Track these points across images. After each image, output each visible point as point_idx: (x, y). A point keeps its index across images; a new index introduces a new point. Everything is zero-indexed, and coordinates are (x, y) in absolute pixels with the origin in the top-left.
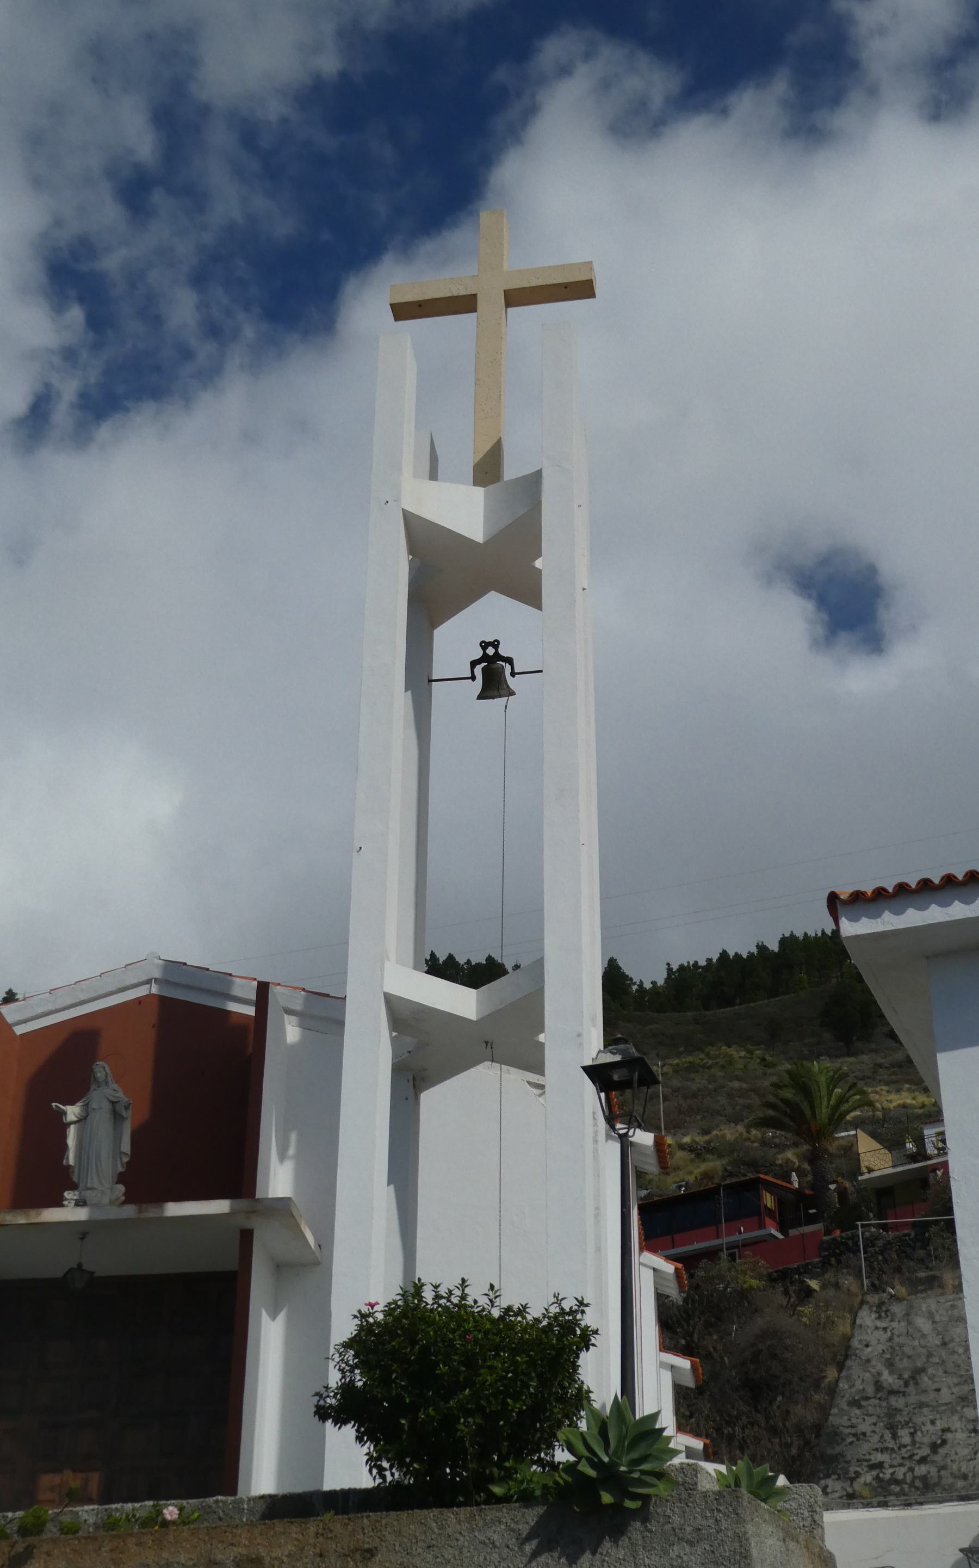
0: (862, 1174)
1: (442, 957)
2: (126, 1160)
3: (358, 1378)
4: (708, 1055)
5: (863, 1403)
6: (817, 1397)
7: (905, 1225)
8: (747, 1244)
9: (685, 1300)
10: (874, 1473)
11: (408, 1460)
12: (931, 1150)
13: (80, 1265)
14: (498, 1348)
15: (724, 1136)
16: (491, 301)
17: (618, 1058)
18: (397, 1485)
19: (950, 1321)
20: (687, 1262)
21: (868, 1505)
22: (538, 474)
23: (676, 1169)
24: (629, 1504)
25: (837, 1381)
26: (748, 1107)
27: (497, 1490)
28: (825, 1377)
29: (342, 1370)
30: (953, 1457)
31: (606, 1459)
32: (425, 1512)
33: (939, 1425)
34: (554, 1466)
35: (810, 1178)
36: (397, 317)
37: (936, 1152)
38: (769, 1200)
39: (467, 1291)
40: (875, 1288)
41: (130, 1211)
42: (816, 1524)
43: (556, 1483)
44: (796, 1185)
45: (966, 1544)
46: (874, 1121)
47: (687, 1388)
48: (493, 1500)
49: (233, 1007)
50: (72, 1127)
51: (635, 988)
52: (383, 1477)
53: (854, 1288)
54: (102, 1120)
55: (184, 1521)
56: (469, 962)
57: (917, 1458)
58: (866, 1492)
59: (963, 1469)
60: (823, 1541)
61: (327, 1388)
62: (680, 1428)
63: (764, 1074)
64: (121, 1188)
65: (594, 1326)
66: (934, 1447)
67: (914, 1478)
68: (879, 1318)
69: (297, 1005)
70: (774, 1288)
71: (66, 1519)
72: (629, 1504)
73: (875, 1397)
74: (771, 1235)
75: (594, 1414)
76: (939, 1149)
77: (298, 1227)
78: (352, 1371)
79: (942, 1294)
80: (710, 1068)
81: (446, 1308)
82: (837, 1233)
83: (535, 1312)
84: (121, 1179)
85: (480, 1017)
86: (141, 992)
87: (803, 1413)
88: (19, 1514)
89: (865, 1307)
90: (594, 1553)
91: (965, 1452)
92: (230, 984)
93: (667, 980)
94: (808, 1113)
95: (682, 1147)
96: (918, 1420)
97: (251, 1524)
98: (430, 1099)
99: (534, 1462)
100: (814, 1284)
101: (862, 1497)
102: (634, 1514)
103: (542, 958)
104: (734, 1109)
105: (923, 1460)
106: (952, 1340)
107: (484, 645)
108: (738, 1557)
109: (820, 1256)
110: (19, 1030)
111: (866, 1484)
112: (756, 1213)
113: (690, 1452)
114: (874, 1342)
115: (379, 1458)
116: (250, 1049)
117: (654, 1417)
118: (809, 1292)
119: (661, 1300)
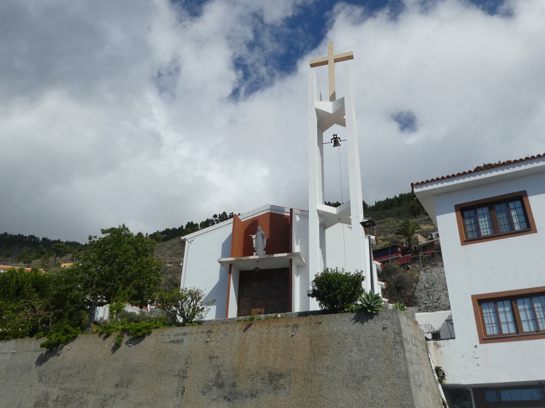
0: (419, 243)
1: (327, 202)
2: (265, 246)
3: (316, 288)
4: (385, 220)
5: (422, 291)
6: (412, 290)
7: (429, 253)
8: (395, 259)
9: (382, 271)
10: (425, 305)
11: (327, 304)
12: (434, 237)
13: (257, 267)
14: (345, 281)
15: (389, 237)
16: (331, 62)
17: (367, 220)
18: (325, 309)
19: (440, 273)
20: (383, 263)
21: (424, 312)
22: (344, 98)
23: (379, 244)
24: (374, 312)
25: (416, 286)
26: (394, 230)
27: (346, 310)
28: (413, 285)
29: (313, 287)
30: (442, 301)
31: (369, 303)
32: (331, 314)
33: (439, 295)
34: (358, 305)
35: (408, 244)
36: (311, 67)
37: (435, 238)
38: (399, 250)
39: (338, 269)
40: (423, 267)
41: (267, 256)
42: (414, 315)
43: (358, 308)
44: (405, 246)
45: (446, 319)
46: (421, 232)
47: (384, 289)
48: (345, 312)
49: (285, 214)
50: (254, 239)
51: (368, 207)
52: (322, 308)
53: (419, 267)
54: (260, 238)
55: (282, 317)
56: (333, 203)
57: (434, 302)
58: (423, 309)
59: (444, 304)
60: (415, 319)
61: (310, 290)
62: (383, 297)
63: (397, 223)
64: (265, 251)
65: (364, 276)
66: (438, 299)
67: (433, 306)
68: (425, 273)
69: (299, 213)
70: (401, 267)
71: (258, 317)
72: (374, 312)
73: (424, 289)
74: (400, 257)
75: (366, 294)
76: (436, 237)
77: (302, 258)
78: (315, 287)
79: (438, 267)
80: (385, 223)
81: (333, 273)
82: (414, 256)
83: (352, 273)
84: (265, 250)
85: (338, 212)
86: (266, 212)
87: (408, 293)
88: (249, 316)
89: (421, 271)
90: (367, 322)
91: (444, 300)
92: (284, 209)
93: (375, 205)
94: (407, 231)
95: (380, 239)
96: (434, 294)
97: (295, 318)
98: (327, 231)
99: (353, 304)
100: (410, 266)
101: (422, 310)
102: (375, 314)
103: (349, 201)
104: (391, 231)
105: (435, 302)
106: (441, 277)
107: (334, 135)
108: (397, 322)
109: (411, 261)
110: (242, 221)
111: (423, 307)
112: (397, 252)
113: (385, 302)
114: (423, 278)
115: (321, 304)
116: (289, 222)
117: (378, 294)
118: (409, 268)
119: (378, 270)
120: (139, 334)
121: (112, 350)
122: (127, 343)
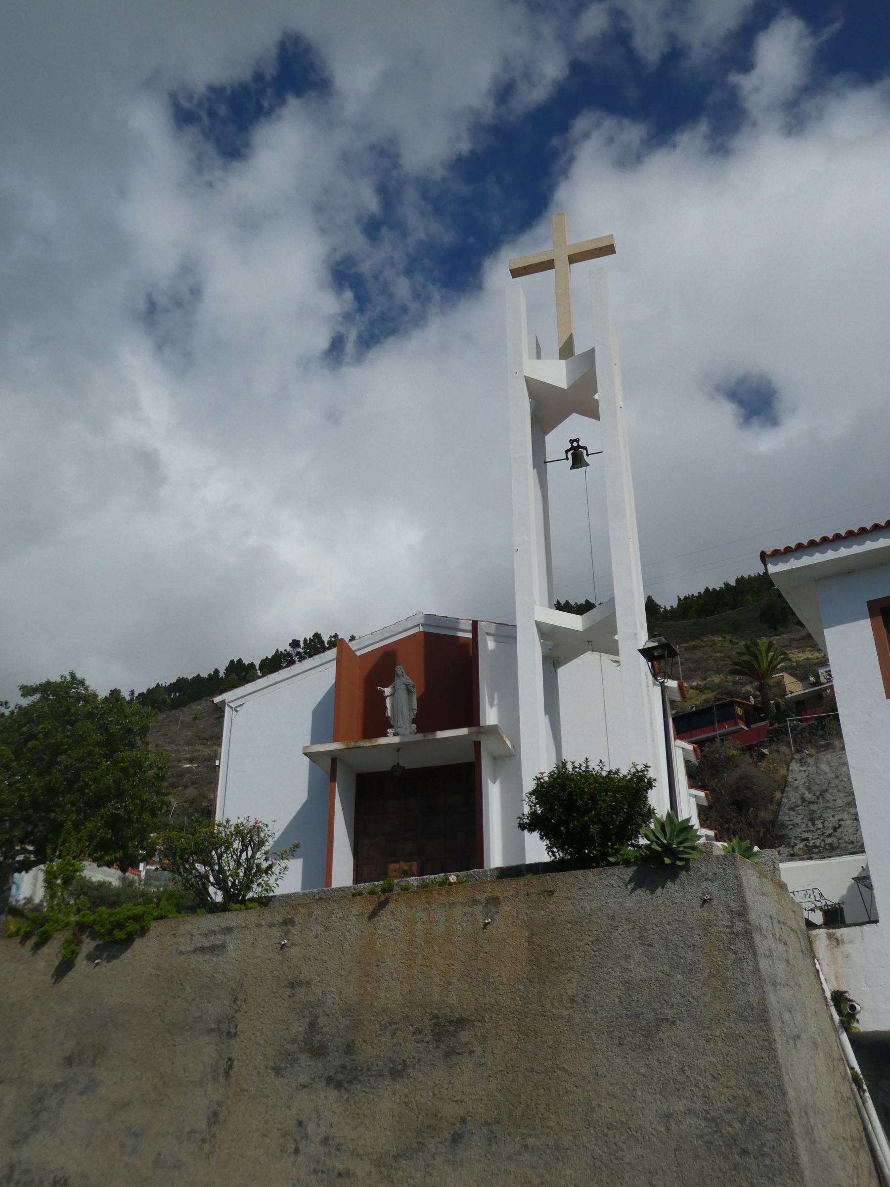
2: (415, 712)
86: (415, 630)
107: (572, 441)
120: (120, 934)
121: (53, 976)
122: (90, 957)
